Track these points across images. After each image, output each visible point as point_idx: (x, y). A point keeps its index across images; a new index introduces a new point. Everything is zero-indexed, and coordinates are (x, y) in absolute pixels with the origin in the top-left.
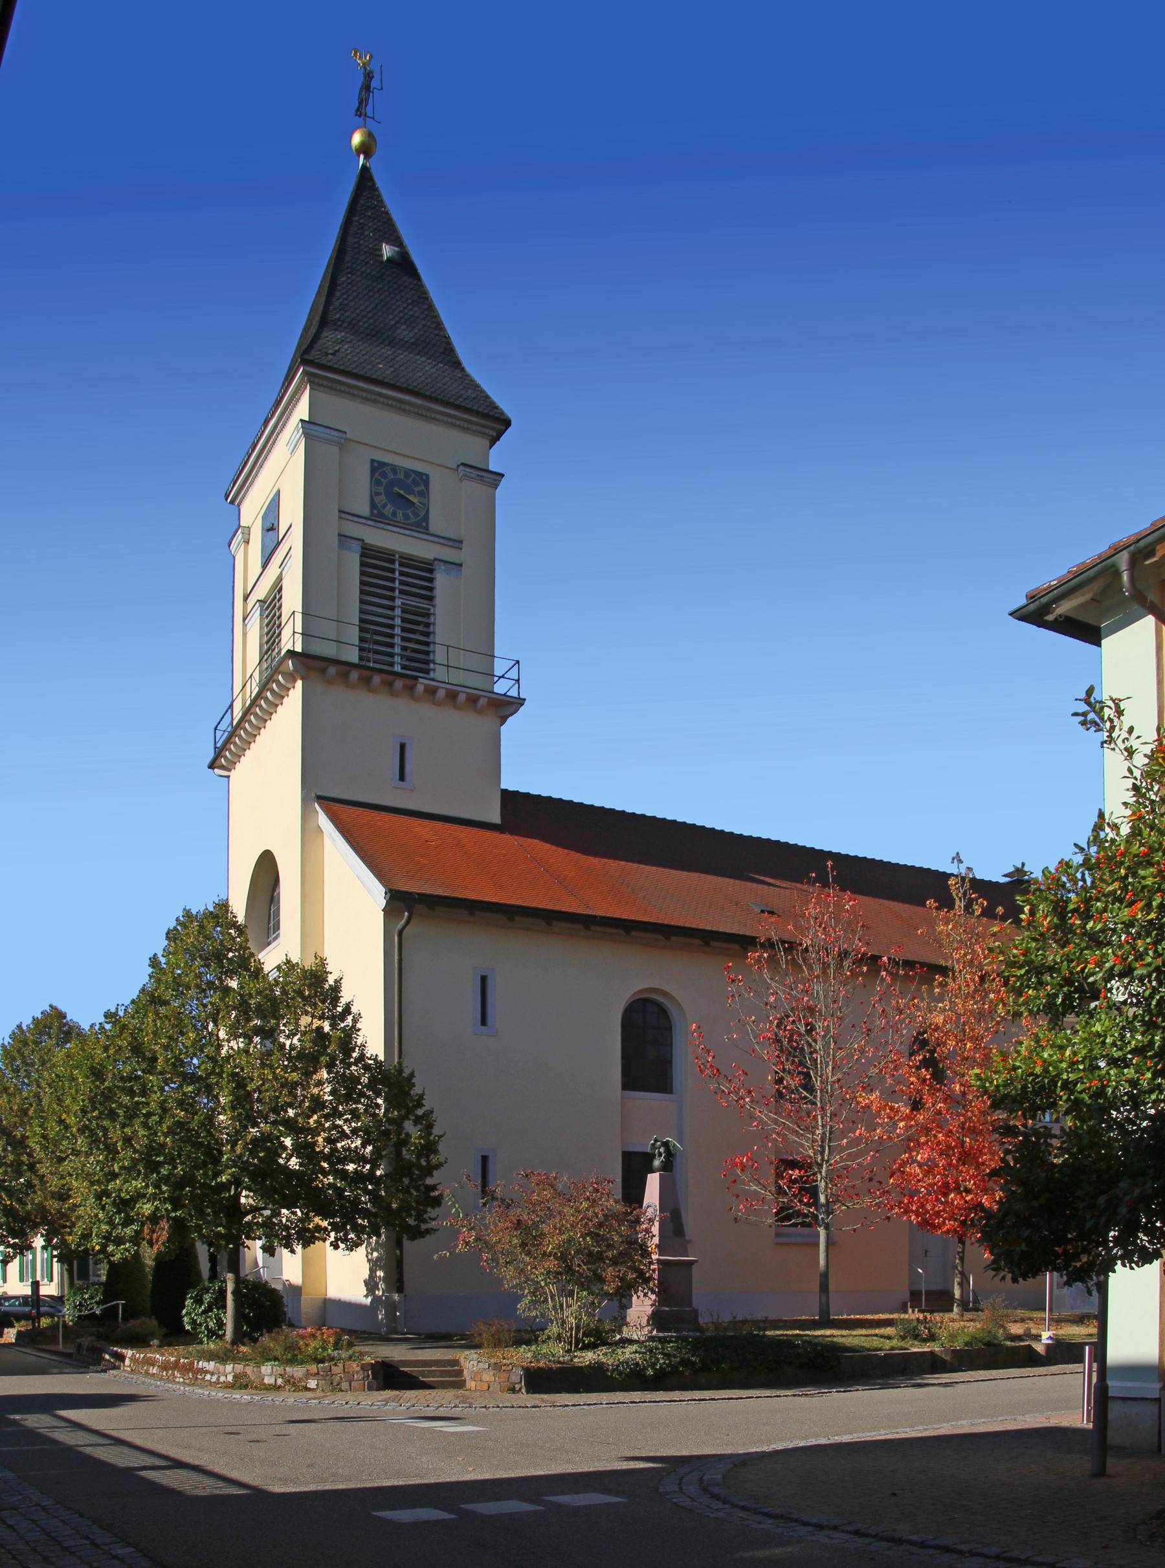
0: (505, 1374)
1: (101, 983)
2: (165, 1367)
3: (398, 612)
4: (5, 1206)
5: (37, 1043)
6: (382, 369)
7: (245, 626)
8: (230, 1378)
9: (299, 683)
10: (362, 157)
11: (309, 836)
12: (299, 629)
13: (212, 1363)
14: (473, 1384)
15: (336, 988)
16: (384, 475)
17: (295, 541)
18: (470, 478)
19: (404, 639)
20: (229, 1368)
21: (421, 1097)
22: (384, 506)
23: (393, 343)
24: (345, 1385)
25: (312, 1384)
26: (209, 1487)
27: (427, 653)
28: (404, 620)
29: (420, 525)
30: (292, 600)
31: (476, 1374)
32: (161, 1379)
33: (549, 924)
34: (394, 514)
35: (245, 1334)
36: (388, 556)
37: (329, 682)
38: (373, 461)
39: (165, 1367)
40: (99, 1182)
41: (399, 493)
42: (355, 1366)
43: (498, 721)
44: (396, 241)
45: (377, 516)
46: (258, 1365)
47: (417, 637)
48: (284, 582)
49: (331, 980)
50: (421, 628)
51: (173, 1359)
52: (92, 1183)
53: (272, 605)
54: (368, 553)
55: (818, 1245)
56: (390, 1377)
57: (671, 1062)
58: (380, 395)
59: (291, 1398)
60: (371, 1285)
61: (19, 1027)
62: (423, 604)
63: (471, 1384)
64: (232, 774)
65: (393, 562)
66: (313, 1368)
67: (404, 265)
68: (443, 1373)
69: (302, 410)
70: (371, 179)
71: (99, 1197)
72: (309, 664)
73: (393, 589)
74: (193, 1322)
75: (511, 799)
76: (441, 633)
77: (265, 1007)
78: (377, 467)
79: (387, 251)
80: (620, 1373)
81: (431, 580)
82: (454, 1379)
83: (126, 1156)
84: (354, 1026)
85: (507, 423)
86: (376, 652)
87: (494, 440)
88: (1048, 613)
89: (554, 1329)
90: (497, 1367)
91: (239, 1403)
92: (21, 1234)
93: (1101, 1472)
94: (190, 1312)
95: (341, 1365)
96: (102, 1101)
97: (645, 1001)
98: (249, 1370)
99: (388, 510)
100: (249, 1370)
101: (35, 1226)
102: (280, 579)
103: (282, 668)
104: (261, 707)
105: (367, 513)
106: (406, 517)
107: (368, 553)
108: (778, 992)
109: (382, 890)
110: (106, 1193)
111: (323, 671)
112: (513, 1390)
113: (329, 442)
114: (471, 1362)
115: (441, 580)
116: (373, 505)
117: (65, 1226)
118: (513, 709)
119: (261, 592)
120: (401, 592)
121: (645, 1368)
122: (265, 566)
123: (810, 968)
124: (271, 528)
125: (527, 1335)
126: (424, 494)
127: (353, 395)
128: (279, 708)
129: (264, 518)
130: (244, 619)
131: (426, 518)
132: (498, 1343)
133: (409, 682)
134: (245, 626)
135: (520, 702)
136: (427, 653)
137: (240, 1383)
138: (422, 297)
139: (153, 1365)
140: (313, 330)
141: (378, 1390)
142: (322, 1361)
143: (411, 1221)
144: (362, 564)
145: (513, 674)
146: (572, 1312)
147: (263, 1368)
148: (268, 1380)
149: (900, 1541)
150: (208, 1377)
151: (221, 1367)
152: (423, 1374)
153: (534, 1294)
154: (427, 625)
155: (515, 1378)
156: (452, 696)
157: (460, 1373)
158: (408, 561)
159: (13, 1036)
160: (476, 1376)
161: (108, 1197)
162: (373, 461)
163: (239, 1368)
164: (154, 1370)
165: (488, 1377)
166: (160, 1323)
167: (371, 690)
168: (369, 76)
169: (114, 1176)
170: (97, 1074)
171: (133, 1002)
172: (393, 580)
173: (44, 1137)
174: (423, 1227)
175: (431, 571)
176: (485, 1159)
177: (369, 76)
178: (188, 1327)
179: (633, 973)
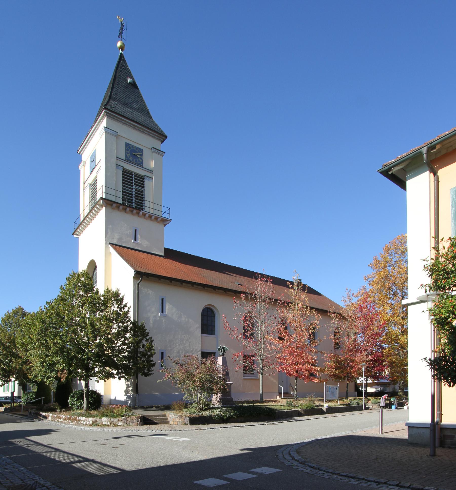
0: (183, 419)
1: (36, 299)
2: (65, 419)
3: (134, 190)
4: (2, 368)
5: (14, 317)
6: (128, 115)
7: (84, 192)
8: (91, 423)
9: (104, 208)
10: (121, 50)
11: (107, 254)
12: (104, 191)
13: (84, 418)
14: (173, 423)
15: (122, 299)
16: (130, 148)
17: (102, 165)
18: (155, 152)
19: (135, 199)
20: (90, 419)
21: (148, 333)
22: (130, 157)
23: (131, 108)
24: (131, 424)
25: (120, 424)
26: (105, 471)
27: (143, 204)
28: (135, 193)
29: (140, 164)
30: (101, 183)
31: (174, 419)
32: (64, 423)
33: (182, 284)
34: (133, 160)
35: (90, 407)
36: (131, 173)
37: (113, 209)
38: (126, 143)
39: (65, 419)
40: (42, 358)
41: (134, 154)
42: (134, 418)
43: (164, 226)
44: (132, 77)
45: (127, 160)
46: (101, 418)
47: (139, 198)
48: (98, 178)
49: (121, 296)
50: (140, 196)
51: (68, 416)
52: (40, 358)
53: (94, 186)
54: (125, 172)
55: (259, 379)
56: (145, 421)
57: (214, 326)
58: (129, 123)
59: (115, 429)
60: (127, 392)
61: (8, 312)
62: (141, 189)
63: (171, 422)
64: (80, 237)
65: (132, 175)
66: (120, 418)
67: (134, 85)
68: (161, 419)
69: (104, 123)
70: (124, 60)
71: (42, 363)
72: (108, 202)
73: (132, 183)
74: (72, 404)
75: (166, 250)
76: (147, 197)
77: (98, 304)
78: (127, 145)
79: (129, 80)
80: (217, 418)
81: (144, 182)
82: (165, 421)
83: (54, 349)
84: (128, 311)
85: (166, 137)
86: (128, 199)
87: (162, 142)
88: (390, 171)
89: (195, 404)
90: (181, 417)
91: (96, 432)
92: (8, 377)
93: (434, 455)
94: (71, 401)
95: (130, 417)
96: (44, 331)
97: (208, 308)
98: (98, 420)
99: (131, 159)
100: (98, 420)
101: (13, 374)
102: (96, 177)
103: (98, 203)
104: (91, 215)
105: (124, 159)
106: (136, 161)
107: (125, 172)
108: (248, 306)
109: (133, 271)
110: (45, 362)
111: (112, 205)
112: (185, 424)
113: (113, 135)
114: (171, 415)
115: (147, 182)
116: (126, 156)
117: (29, 373)
118: (168, 222)
119: (90, 181)
120: (135, 184)
121: (224, 416)
122: (91, 173)
123: (257, 300)
124: (93, 160)
125: (187, 405)
126: (142, 155)
127: (120, 121)
128: (97, 216)
129: (91, 158)
130: (84, 190)
131: (142, 162)
132: (180, 409)
133: (138, 211)
134: (84, 192)
135: (170, 220)
136: (143, 204)
137: (94, 424)
138: (140, 96)
139: (61, 418)
140: (106, 101)
141: (142, 425)
142: (123, 416)
143: (146, 371)
144: (123, 174)
145: (168, 212)
146: (201, 399)
147: (103, 419)
148: (105, 423)
149: (346, 476)
150: (82, 422)
151: (87, 419)
152: (155, 419)
153: (188, 393)
154: (143, 195)
155: (186, 420)
156: (150, 217)
157: (167, 419)
158: (137, 175)
159: (6, 315)
160: (173, 420)
161: (45, 363)
162: (126, 143)
163: (94, 419)
164: (61, 420)
165: (178, 420)
166: (59, 404)
167: (126, 212)
168: (123, 25)
169: (47, 356)
170: (43, 322)
171: (55, 299)
172: (132, 180)
173: (23, 343)
174: (150, 373)
175: (144, 179)
176: (162, 353)
177: (123, 25)
178: (70, 405)
179: (204, 300)
